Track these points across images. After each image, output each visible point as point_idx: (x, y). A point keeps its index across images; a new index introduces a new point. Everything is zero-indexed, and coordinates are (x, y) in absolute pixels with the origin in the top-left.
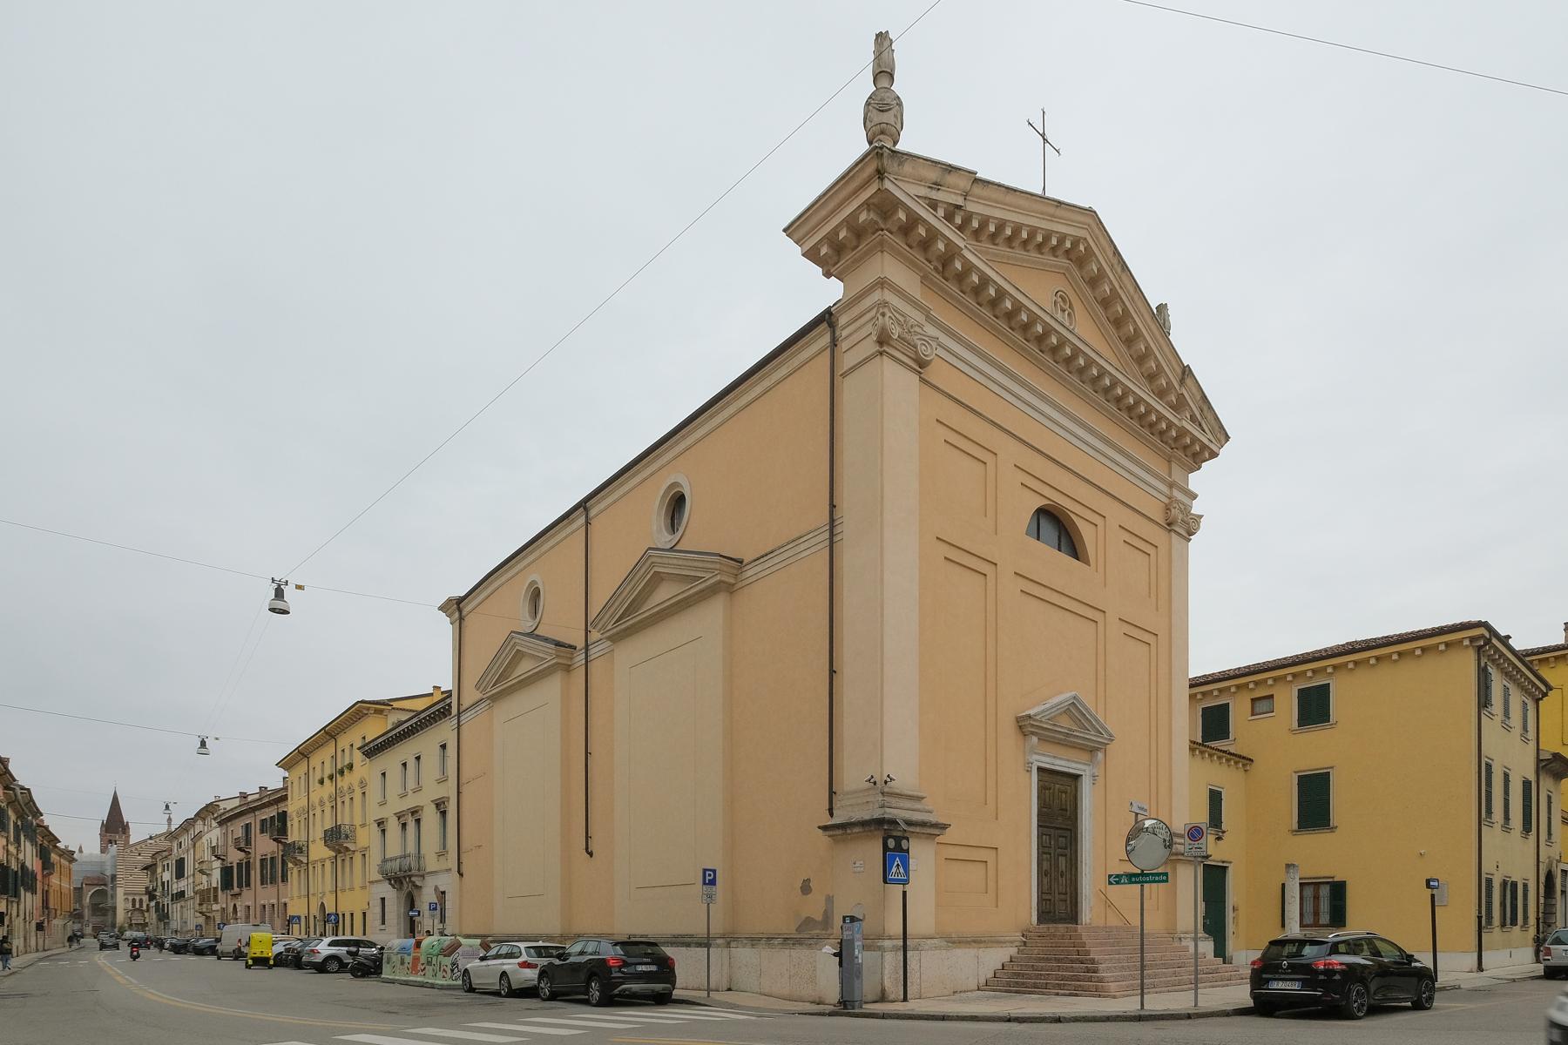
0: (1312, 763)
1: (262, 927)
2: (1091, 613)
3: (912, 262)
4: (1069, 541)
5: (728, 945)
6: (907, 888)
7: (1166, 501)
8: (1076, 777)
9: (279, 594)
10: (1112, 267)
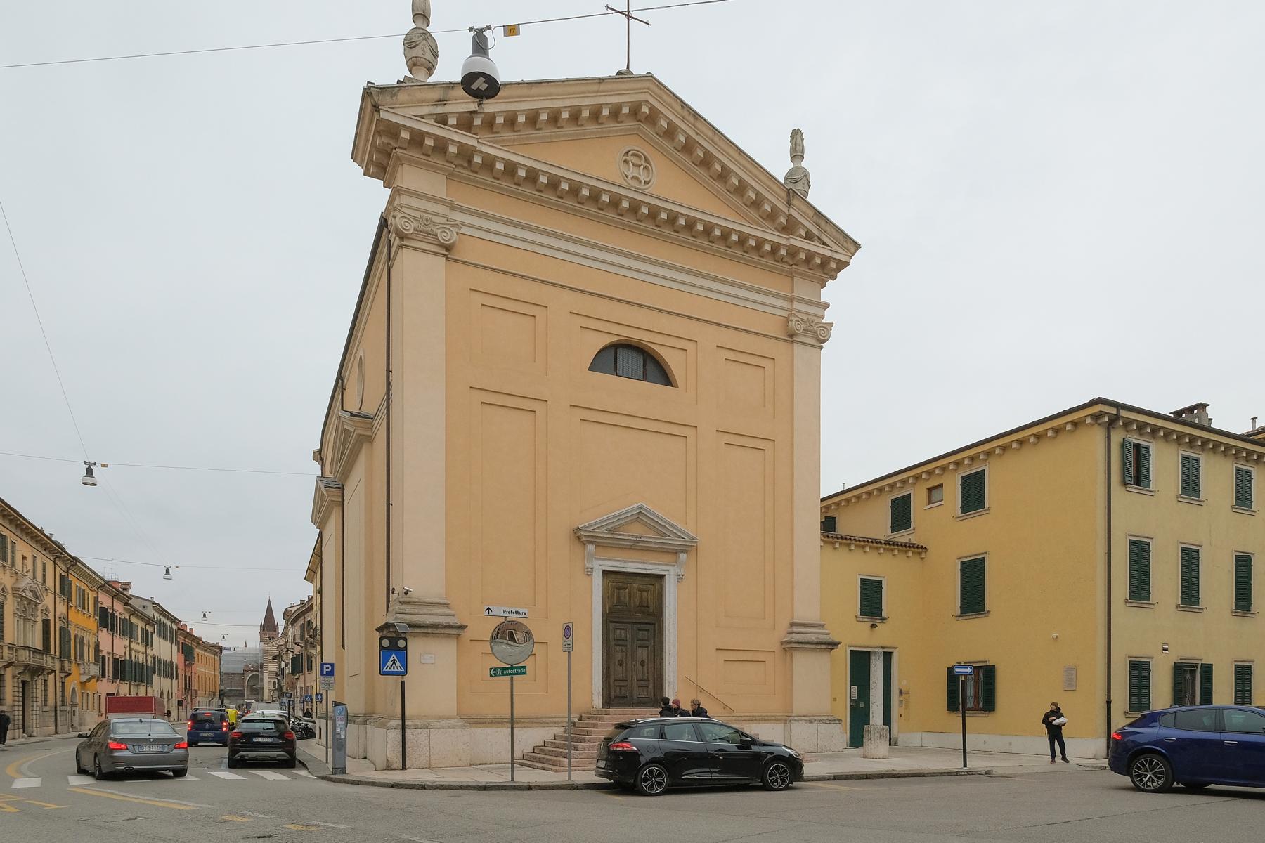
0: (970, 550)
1: (273, 704)
2: (680, 430)
3: (432, 167)
4: (653, 367)
5: (365, 723)
6: (405, 678)
7: (785, 314)
8: (663, 576)
9: (89, 472)
10: (683, 119)
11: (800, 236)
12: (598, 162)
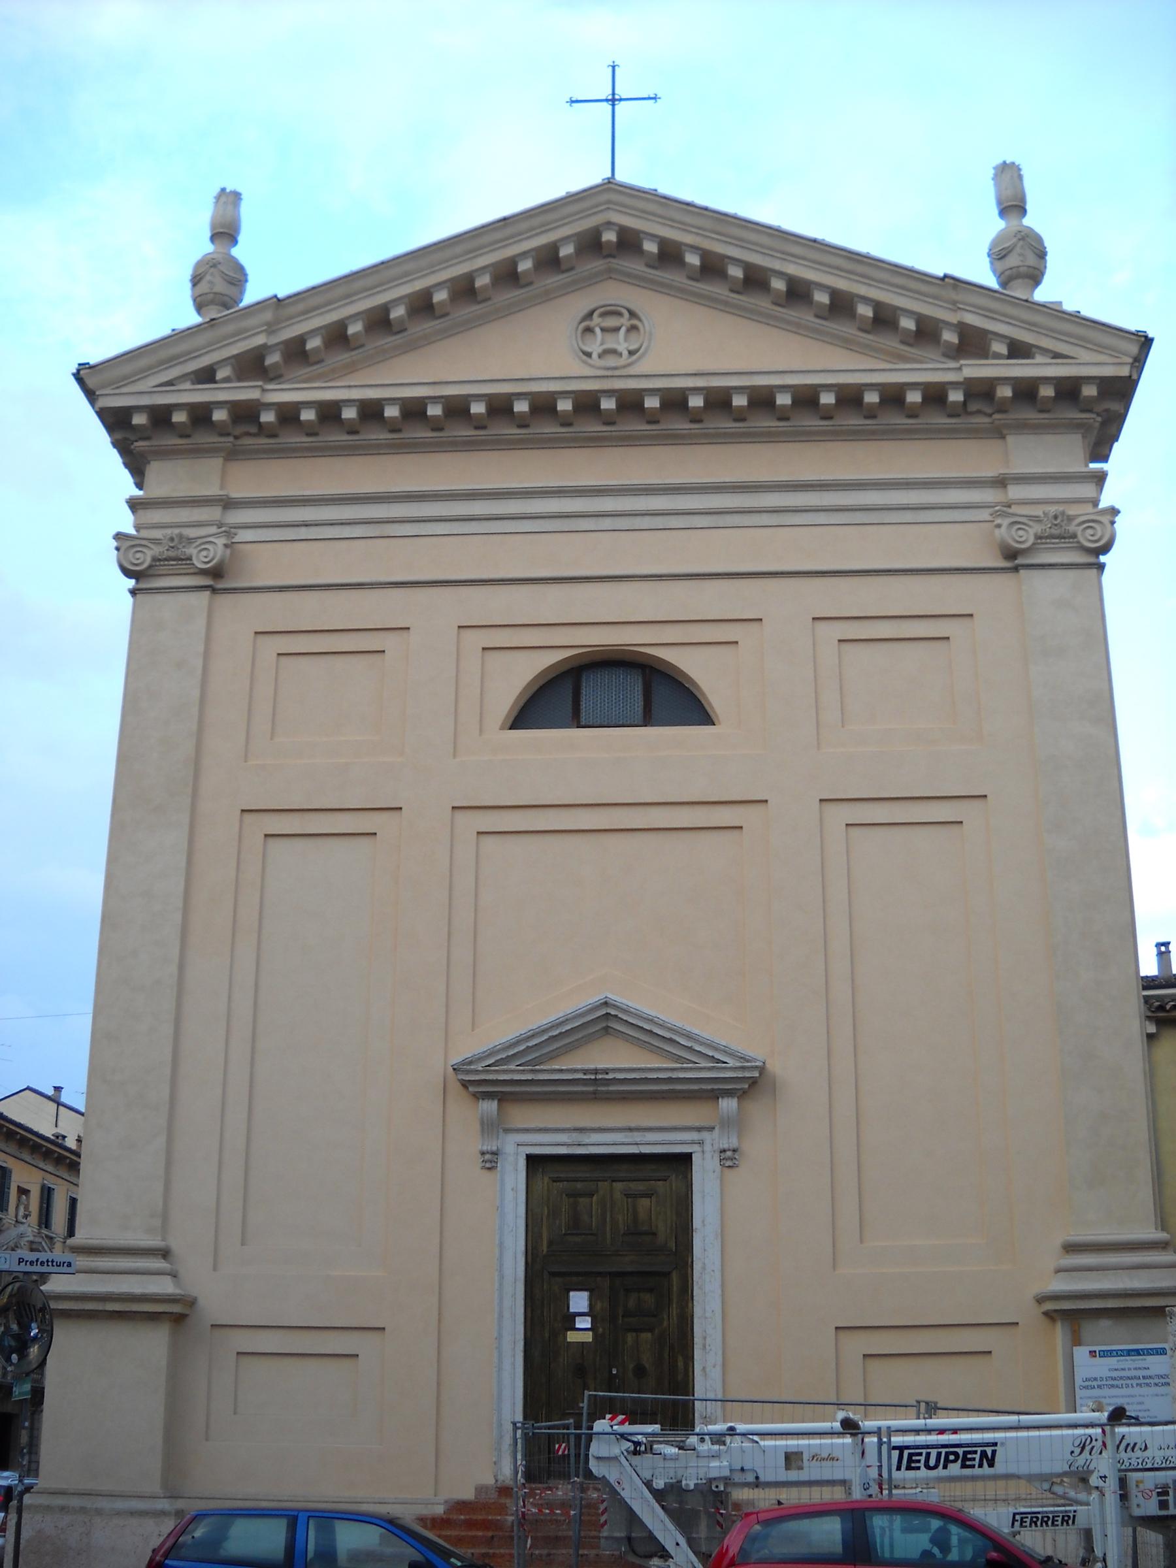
8: (687, 1158)
11: (997, 356)
12: (538, 352)
